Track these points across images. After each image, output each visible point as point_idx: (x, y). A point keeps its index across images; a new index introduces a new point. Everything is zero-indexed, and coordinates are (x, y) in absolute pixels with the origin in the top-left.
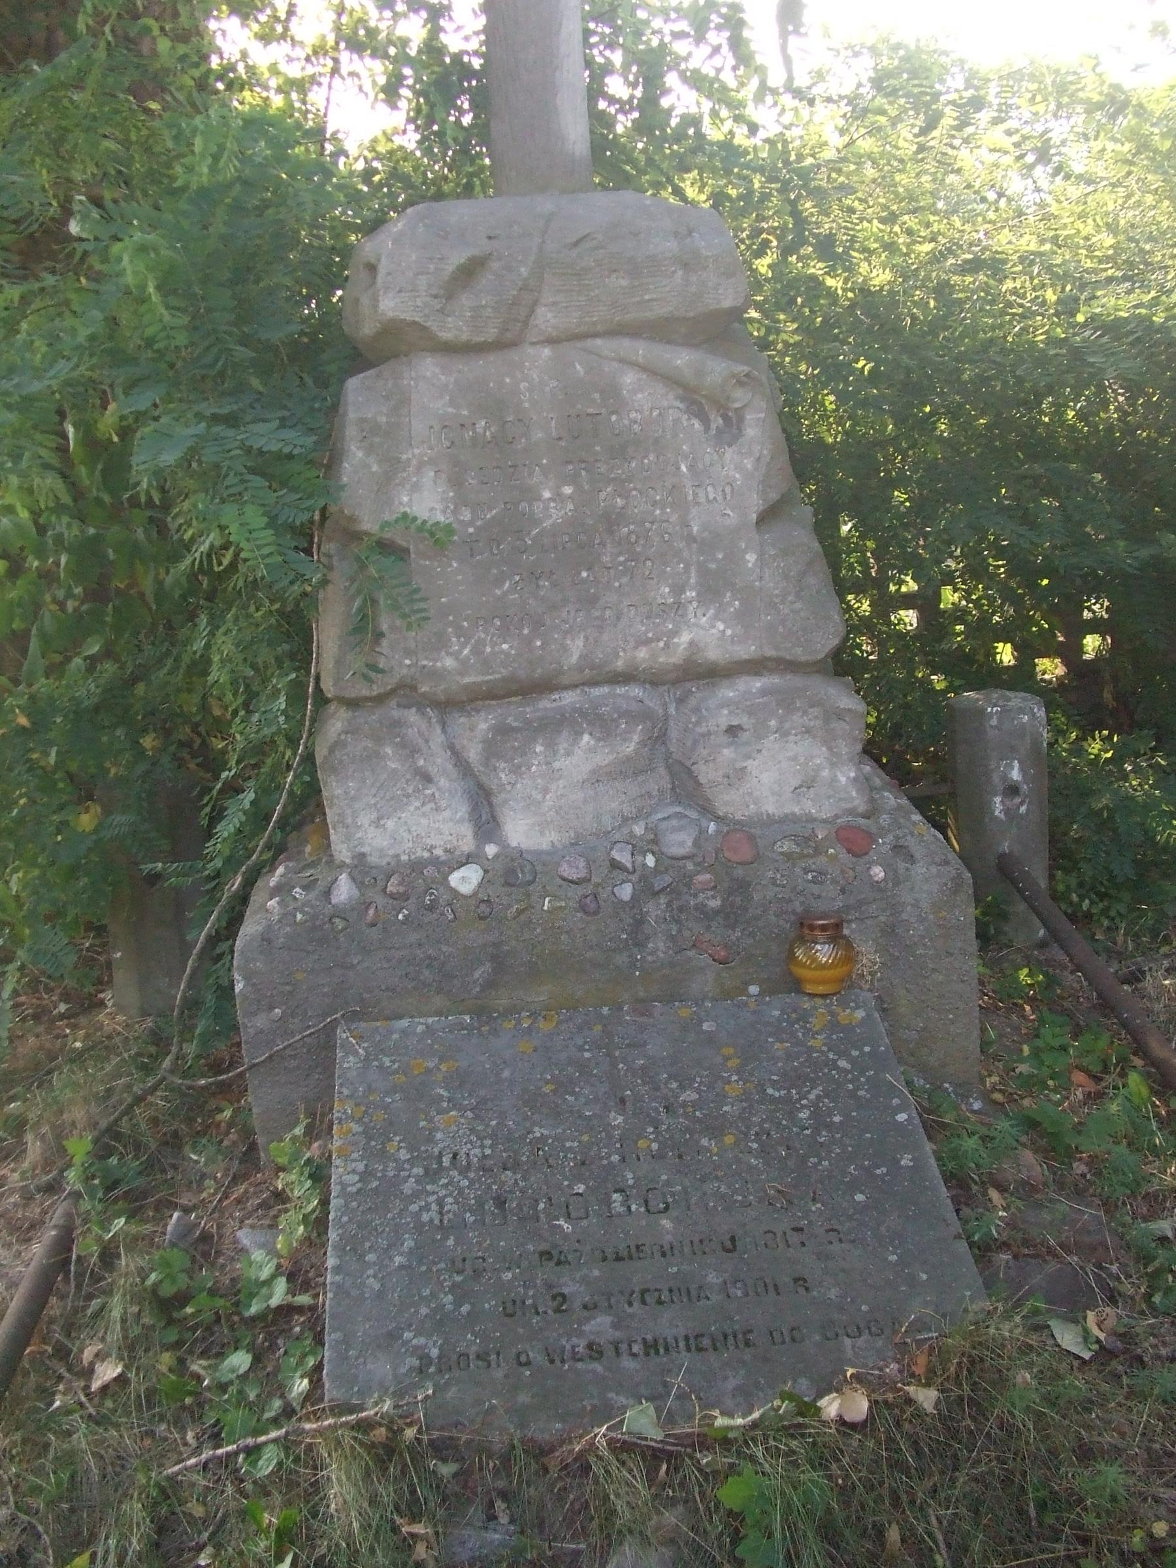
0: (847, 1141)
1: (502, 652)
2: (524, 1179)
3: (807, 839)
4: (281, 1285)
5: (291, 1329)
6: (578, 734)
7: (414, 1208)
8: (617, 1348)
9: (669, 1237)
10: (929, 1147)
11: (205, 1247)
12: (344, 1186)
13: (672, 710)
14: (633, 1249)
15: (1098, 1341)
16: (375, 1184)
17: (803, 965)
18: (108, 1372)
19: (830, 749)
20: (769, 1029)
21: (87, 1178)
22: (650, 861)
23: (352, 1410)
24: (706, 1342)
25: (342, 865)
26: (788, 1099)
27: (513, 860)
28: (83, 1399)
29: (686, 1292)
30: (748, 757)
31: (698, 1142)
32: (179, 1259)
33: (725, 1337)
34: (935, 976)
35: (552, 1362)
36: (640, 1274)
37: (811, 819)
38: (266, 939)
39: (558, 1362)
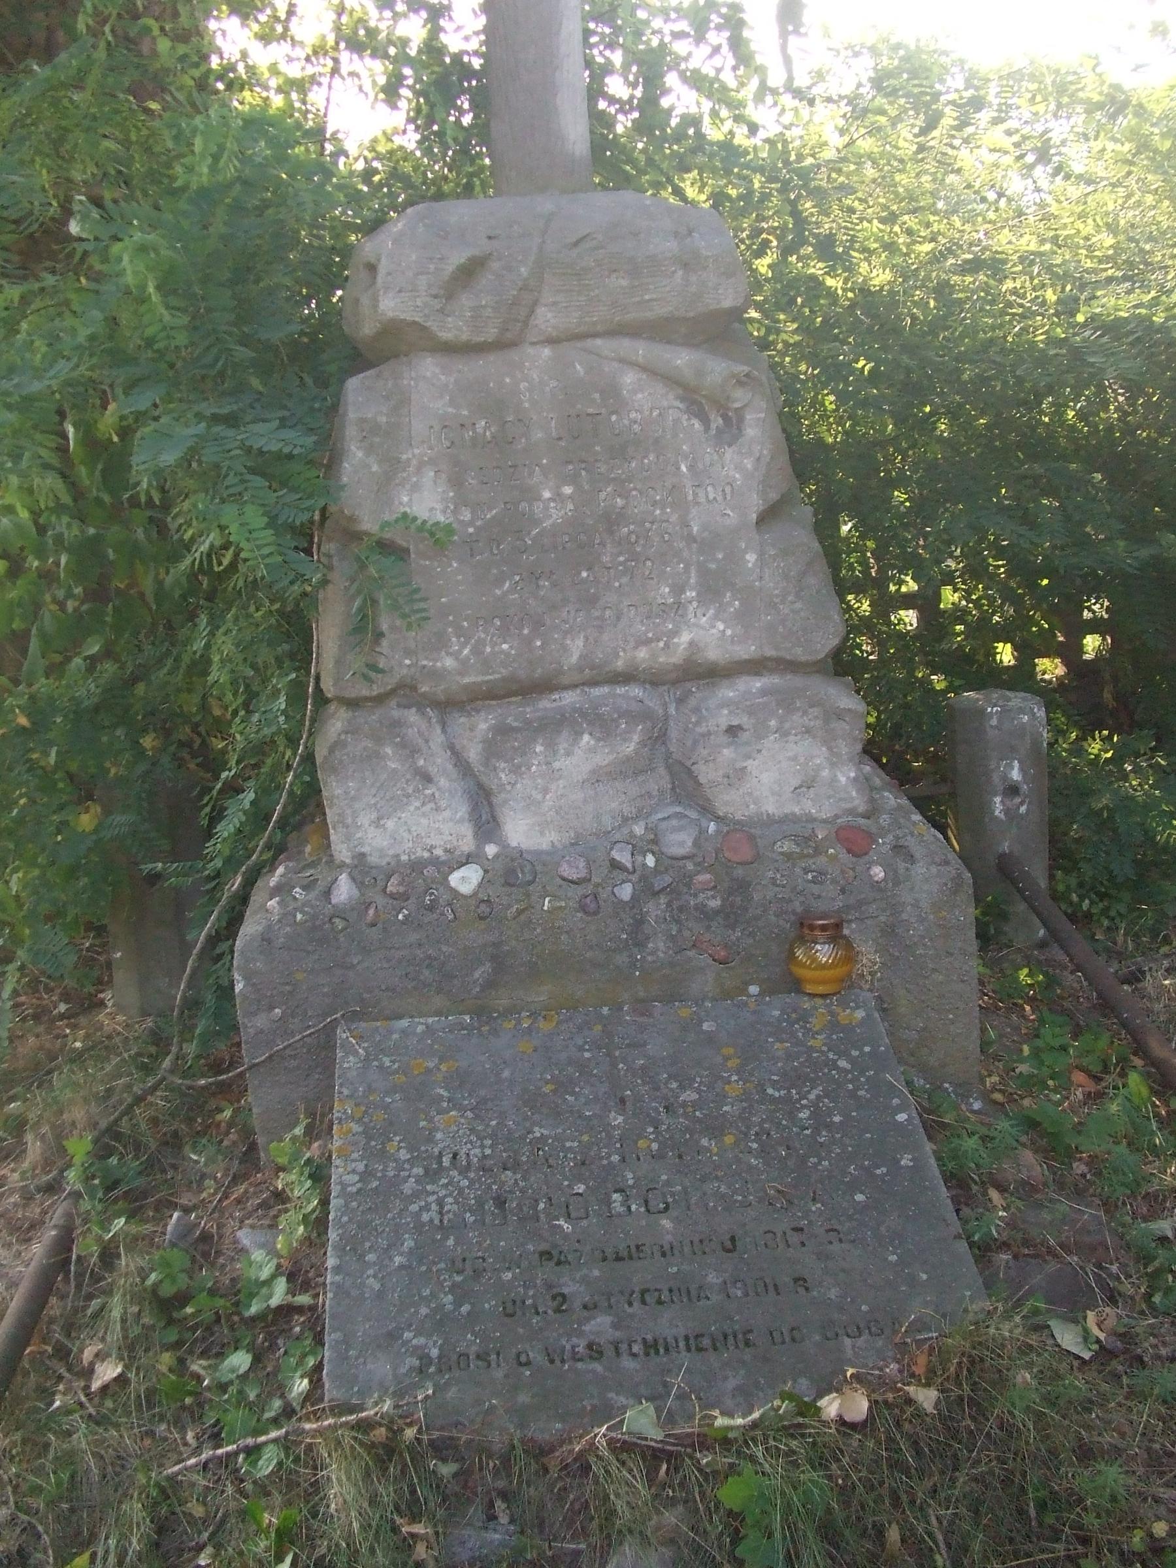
0: (847, 1141)
1: (502, 652)
2: (524, 1179)
3: (807, 839)
4: (281, 1285)
5: (291, 1329)
6: (578, 734)
7: (414, 1208)
8: (617, 1348)
9: (669, 1237)
10: (929, 1147)
11: (205, 1247)
12: (344, 1186)
13: (672, 710)
14: (633, 1249)
15: (1098, 1341)
16: (375, 1184)
17: (803, 965)
18: (108, 1372)
19: (830, 749)
20: (769, 1029)
21: (87, 1178)
22: (650, 861)
23: (352, 1410)
24: (706, 1342)
25: (342, 865)
26: (788, 1099)
27: (513, 860)
28: (83, 1399)
29: (686, 1292)
30: (748, 757)
31: (698, 1142)
32: (179, 1259)
33: (725, 1337)
34: (935, 976)
35: (552, 1362)
36: (640, 1274)
37: (811, 819)
38: (266, 939)
39: (558, 1362)
